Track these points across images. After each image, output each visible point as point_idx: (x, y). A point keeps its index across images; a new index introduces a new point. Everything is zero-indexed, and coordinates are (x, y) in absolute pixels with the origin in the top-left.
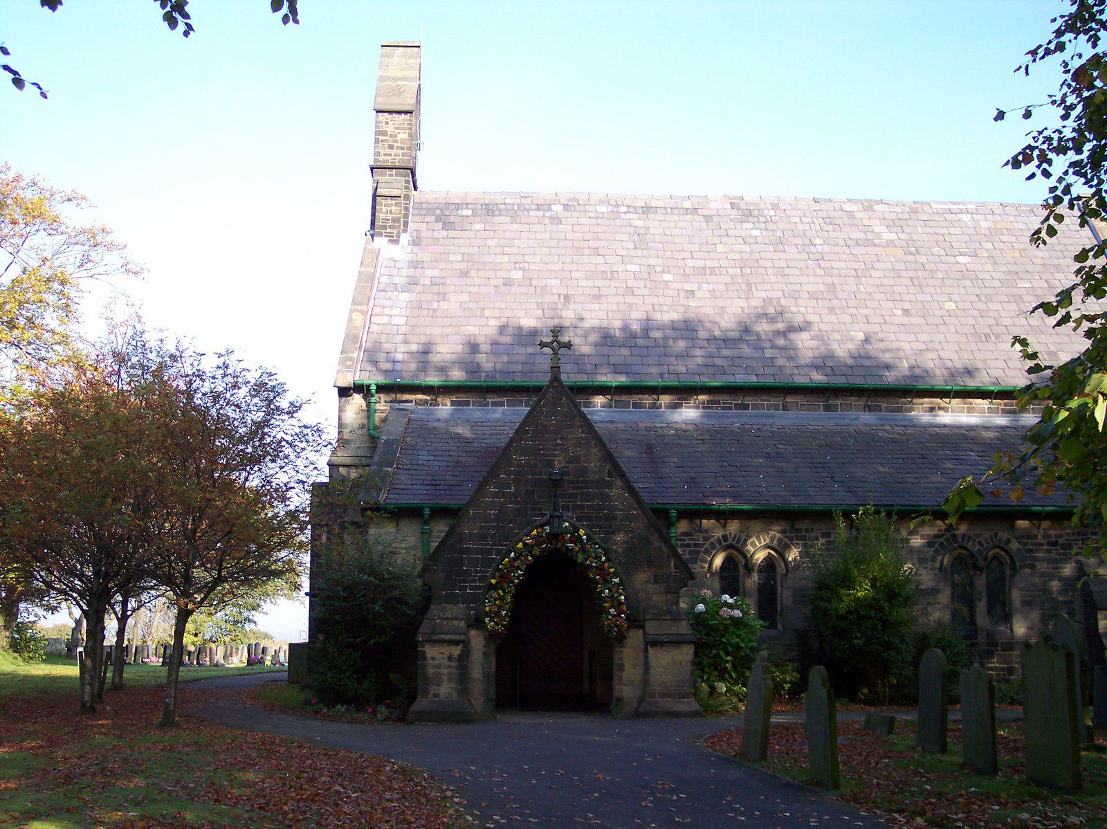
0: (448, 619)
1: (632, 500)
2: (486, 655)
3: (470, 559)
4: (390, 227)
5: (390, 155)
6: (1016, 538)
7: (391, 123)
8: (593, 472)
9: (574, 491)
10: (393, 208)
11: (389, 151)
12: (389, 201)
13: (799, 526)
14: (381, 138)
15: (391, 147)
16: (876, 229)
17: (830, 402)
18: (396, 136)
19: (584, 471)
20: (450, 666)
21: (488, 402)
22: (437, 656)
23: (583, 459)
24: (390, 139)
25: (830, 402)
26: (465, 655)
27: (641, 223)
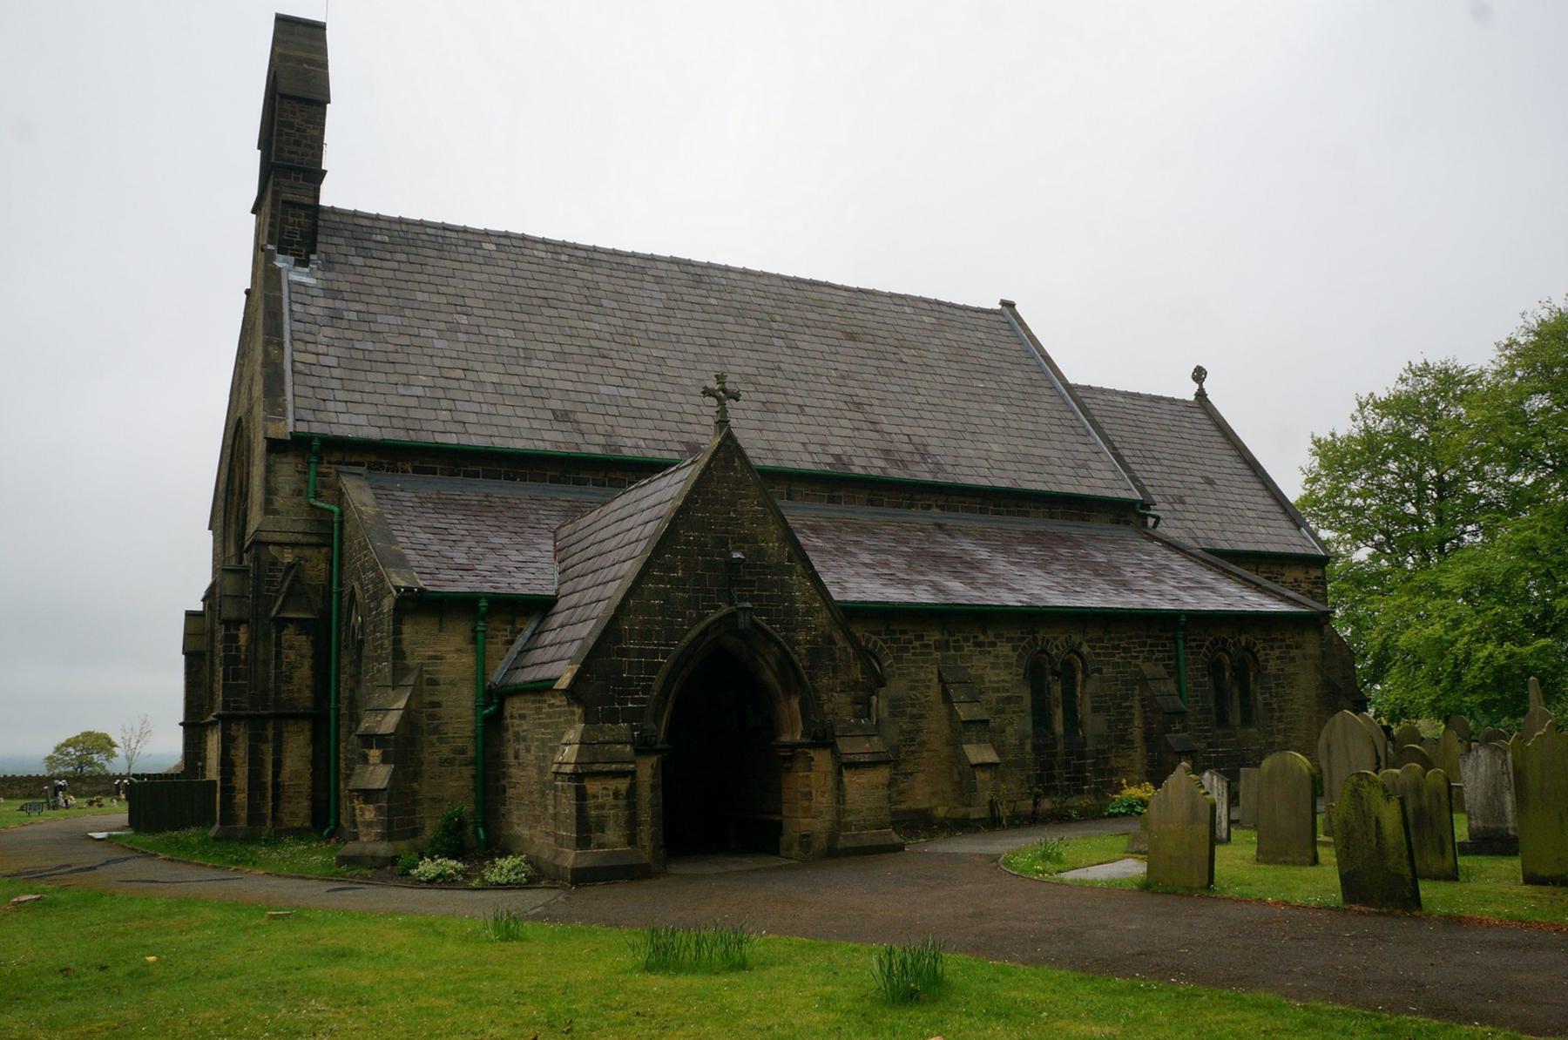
1: (813, 591)
2: (653, 788)
3: (631, 663)
4: (297, 243)
5: (297, 153)
6: (1087, 642)
7: (298, 114)
10: (303, 220)
11: (295, 149)
12: (298, 211)
15: (298, 143)
18: (304, 131)
19: (760, 553)
20: (616, 806)
21: (459, 471)
23: (760, 537)
24: (298, 133)
26: (632, 791)
27: (588, 276)
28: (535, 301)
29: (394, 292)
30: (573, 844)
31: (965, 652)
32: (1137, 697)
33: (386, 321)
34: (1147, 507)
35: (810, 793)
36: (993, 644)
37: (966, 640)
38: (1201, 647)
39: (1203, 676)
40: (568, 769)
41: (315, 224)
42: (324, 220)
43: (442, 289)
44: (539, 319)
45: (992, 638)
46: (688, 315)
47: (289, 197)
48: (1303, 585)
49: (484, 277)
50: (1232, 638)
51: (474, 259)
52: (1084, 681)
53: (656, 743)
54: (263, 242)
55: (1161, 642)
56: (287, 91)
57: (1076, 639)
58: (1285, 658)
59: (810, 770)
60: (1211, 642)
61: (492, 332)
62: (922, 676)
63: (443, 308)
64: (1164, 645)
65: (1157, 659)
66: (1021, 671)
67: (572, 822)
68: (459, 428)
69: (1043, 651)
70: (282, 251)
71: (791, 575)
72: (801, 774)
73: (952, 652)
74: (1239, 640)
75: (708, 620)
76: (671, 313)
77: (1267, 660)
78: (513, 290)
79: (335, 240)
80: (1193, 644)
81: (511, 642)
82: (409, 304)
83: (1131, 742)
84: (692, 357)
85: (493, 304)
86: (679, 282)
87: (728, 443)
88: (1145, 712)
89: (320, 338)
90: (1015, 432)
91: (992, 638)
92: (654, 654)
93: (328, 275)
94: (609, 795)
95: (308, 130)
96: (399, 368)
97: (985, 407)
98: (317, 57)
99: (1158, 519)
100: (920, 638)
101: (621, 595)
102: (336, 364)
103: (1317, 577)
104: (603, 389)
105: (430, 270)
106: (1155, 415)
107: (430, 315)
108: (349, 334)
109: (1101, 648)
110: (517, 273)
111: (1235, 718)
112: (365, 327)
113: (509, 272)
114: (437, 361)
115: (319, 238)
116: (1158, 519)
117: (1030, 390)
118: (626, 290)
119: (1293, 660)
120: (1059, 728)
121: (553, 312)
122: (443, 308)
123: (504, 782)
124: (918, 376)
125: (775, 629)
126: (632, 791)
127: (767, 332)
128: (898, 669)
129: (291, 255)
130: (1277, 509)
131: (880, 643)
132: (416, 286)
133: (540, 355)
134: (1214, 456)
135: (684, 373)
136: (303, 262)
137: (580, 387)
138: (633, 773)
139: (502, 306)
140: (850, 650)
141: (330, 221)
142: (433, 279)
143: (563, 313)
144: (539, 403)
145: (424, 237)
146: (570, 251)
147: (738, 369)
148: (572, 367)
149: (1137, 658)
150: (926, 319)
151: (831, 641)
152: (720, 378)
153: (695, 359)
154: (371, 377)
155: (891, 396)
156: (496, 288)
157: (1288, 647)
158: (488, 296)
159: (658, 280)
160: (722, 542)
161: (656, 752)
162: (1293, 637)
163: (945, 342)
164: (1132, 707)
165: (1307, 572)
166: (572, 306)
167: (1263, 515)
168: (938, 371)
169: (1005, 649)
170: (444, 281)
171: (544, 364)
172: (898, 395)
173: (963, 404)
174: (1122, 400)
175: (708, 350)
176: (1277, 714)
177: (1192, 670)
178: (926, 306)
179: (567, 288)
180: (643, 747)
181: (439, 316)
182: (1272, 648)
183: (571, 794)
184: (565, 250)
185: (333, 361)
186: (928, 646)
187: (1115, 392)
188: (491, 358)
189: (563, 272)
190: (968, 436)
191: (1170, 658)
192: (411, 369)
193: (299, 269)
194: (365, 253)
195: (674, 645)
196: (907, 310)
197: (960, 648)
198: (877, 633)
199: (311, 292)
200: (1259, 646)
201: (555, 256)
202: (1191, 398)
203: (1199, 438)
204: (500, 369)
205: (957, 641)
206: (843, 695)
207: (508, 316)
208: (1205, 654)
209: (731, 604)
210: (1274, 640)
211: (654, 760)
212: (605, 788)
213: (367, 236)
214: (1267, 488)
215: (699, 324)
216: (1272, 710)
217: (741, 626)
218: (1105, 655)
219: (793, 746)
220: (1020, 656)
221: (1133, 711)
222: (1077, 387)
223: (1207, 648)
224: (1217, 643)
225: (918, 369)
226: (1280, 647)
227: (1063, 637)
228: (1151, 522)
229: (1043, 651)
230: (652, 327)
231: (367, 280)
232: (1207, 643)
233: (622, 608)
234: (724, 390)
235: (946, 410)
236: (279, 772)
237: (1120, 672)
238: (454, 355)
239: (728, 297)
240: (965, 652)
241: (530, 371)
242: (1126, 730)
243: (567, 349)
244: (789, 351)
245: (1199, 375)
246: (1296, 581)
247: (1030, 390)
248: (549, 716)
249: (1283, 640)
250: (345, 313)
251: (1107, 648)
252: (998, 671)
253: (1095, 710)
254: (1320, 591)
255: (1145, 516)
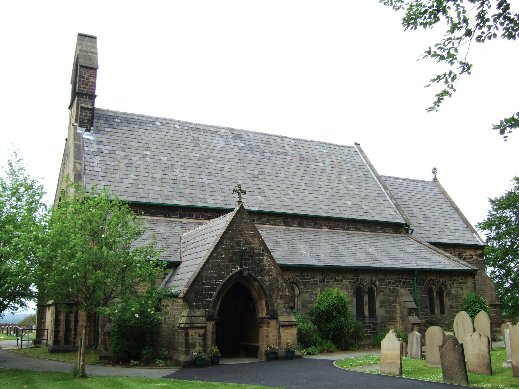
0: (197, 316)
2: (212, 333)
3: (206, 288)
4: (86, 123)
5: (86, 88)
6: (378, 280)
7: (87, 73)
8: (256, 249)
9: (249, 258)
10: (88, 114)
11: (85, 86)
12: (86, 111)
13: (304, 274)
14: (82, 79)
15: (86, 84)
16: (287, 148)
17: (286, 221)
18: (89, 80)
19: (252, 248)
20: (199, 339)
22: (194, 334)
23: (252, 243)
25: (286, 221)
26: (205, 334)
27: (195, 135)
28: (175, 145)
29: (122, 142)
30: (184, 353)
31: (331, 284)
32: (398, 302)
33: (119, 153)
34: (409, 226)
35: (269, 336)
36: (341, 281)
37: (331, 279)
38: (423, 283)
39: (425, 294)
40: (183, 325)
41: (93, 115)
42: (96, 113)
43: (140, 141)
44: (176, 152)
45: (341, 278)
46: (232, 150)
47: (84, 105)
48: (474, 257)
49: (156, 136)
50: (437, 279)
51: (152, 128)
52: (377, 295)
53: (214, 317)
54: (73, 121)
55: (407, 281)
56: (82, 64)
57: (374, 279)
58: (459, 287)
59: (269, 327)
60: (428, 281)
61: (159, 158)
62: (314, 292)
63: (141, 148)
64: (409, 282)
65: (406, 287)
66: (352, 291)
67: (183, 345)
68: (146, 195)
69: (361, 283)
70: (80, 126)
71: (263, 257)
72: (265, 329)
73: (326, 283)
74: (439, 280)
75: (234, 272)
76: (226, 149)
77: (451, 288)
78: (167, 141)
79: (100, 121)
80: (421, 282)
81: (164, 278)
82: (128, 147)
83: (395, 319)
84: (233, 167)
85: (159, 147)
86: (229, 137)
87: (242, 209)
88: (401, 308)
89: (95, 160)
90: (357, 196)
91: (341, 278)
92: (214, 284)
93: (98, 135)
94: (196, 335)
95: (90, 79)
96: (124, 172)
97: (346, 186)
98: (93, 50)
99: (413, 230)
100: (313, 278)
101: (203, 264)
102: (101, 171)
103: (480, 254)
104: (200, 180)
105: (136, 133)
106: (415, 188)
107: (135, 151)
108: (105, 159)
109: (383, 282)
110: (168, 134)
111: (437, 311)
112: (111, 156)
113: (165, 134)
114: (138, 169)
115: (95, 121)
116: (413, 230)
117: (364, 179)
118: (210, 141)
119: (462, 288)
120: (366, 313)
121: (182, 150)
122: (141, 148)
123: (160, 330)
124: (320, 174)
125: (257, 276)
126: (205, 334)
127: (263, 157)
128: (305, 289)
129: (84, 127)
130: (465, 226)
131: (299, 279)
132: (131, 140)
133: (176, 167)
134: (439, 204)
135: (230, 173)
136: (88, 130)
137: (191, 179)
138: (205, 327)
139: (163, 147)
140: (284, 284)
141: (98, 113)
142: (137, 137)
143: (186, 150)
144: (176, 186)
145: (134, 120)
146: (188, 125)
147: (251, 172)
148: (188, 171)
149: (398, 286)
150: (324, 151)
151: (277, 281)
152: (239, 186)
153: (235, 168)
154: (113, 175)
155: (309, 182)
156: (160, 140)
157: (460, 283)
158: (158, 143)
159: (222, 136)
160: (239, 245)
161: (213, 320)
162: (462, 279)
163: (332, 160)
164: (395, 306)
165: (476, 252)
166: (189, 147)
167: (458, 228)
168: (328, 172)
169: (346, 282)
170: (141, 137)
171: (178, 170)
172: (312, 182)
173: (337, 185)
174: (402, 182)
175: (240, 164)
176: (455, 310)
177: (420, 292)
178: (325, 145)
179: (187, 140)
180: (209, 318)
181: (139, 152)
182: (453, 284)
183: (183, 335)
184: (187, 125)
185: (100, 170)
186: (317, 281)
187: (400, 179)
188: (158, 168)
189: (186, 134)
190: (338, 198)
191: (411, 287)
192: (129, 173)
193: (87, 133)
194: (111, 126)
195: (221, 282)
196: (317, 147)
197: (328, 282)
198: (298, 276)
199: (91, 142)
200: (447, 283)
201: (183, 127)
202: (431, 180)
203: (433, 197)
204: (162, 172)
205: (328, 279)
206: (280, 300)
207: (165, 151)
208: (425, 286)
209: (241, 266)
210: (453, 280)
211: (213, 323)
212: (195, 333)
213: (112, 120)
214: (461, 217)
215: (237, 154)
216: (453, 308)
217: (245, 275)
218: (385, 285)
219: (263, 318)
220: (352, 285)
221: (396, 307)
222: (382, 177)
223: (427, 283)
224: (430, 281)
225: (320, 171)
226: (457, 283)
227: (368, 279)
228: (410, 231)
229: (361, 283)
230: (219, 155)
231: (112, 137)
232: (426, 281)
233: (203, 269)
234: (240, 190)
235: (330, 187)
236: (77, 325)
237: (391, 292)
238: (144, 167)
239: (248, 143)
240: (331, 284)
241: (172, 173)
242: (393, 314)
243: (187, 164)
244: (270, 165)
245: (434, 171)
246: (471, 255)
247: (364, 179)
248: (177, 306)
249: (458, 281)
250: (104, 150)
251: (386, 282)
252: (343, 291)
253: (381, 306)
254: (481, 259)
255: (408, 230)
